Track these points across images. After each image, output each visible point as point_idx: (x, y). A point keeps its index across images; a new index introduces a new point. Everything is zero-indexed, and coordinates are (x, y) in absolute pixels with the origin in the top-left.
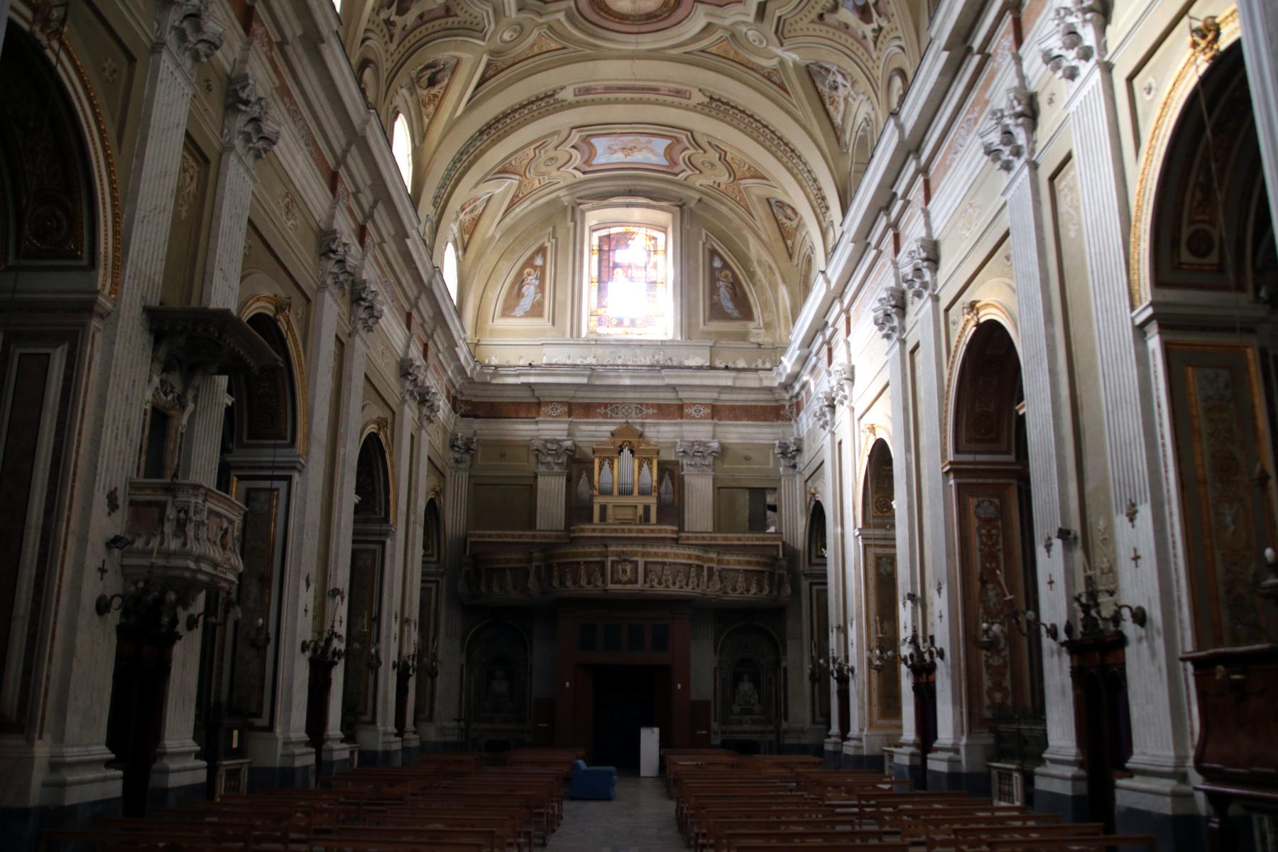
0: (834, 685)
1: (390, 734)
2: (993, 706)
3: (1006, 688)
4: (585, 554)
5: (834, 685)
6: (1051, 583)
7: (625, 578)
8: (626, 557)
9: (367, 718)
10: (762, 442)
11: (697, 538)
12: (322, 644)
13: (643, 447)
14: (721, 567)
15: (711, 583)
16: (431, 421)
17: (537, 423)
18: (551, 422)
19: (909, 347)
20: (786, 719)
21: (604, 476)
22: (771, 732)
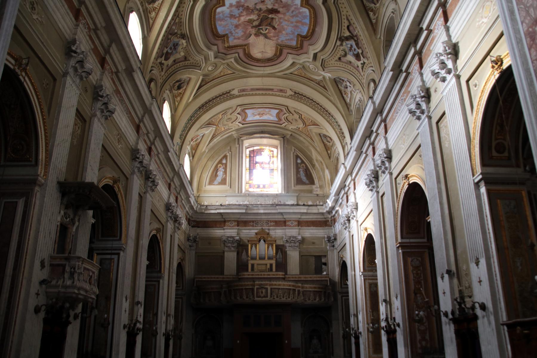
0: (353, 340)
5: (353, 340)
6: (444, 293)
7: (262, 295)
8: (263, 286)
12: (132, 325)
13: (269, 239)
14: (303, 290)
15: (299, 297)
16: (179, 229)
17: (224, 229)
18: (230, 229)
19: (380, 194)
21: (253, 251)
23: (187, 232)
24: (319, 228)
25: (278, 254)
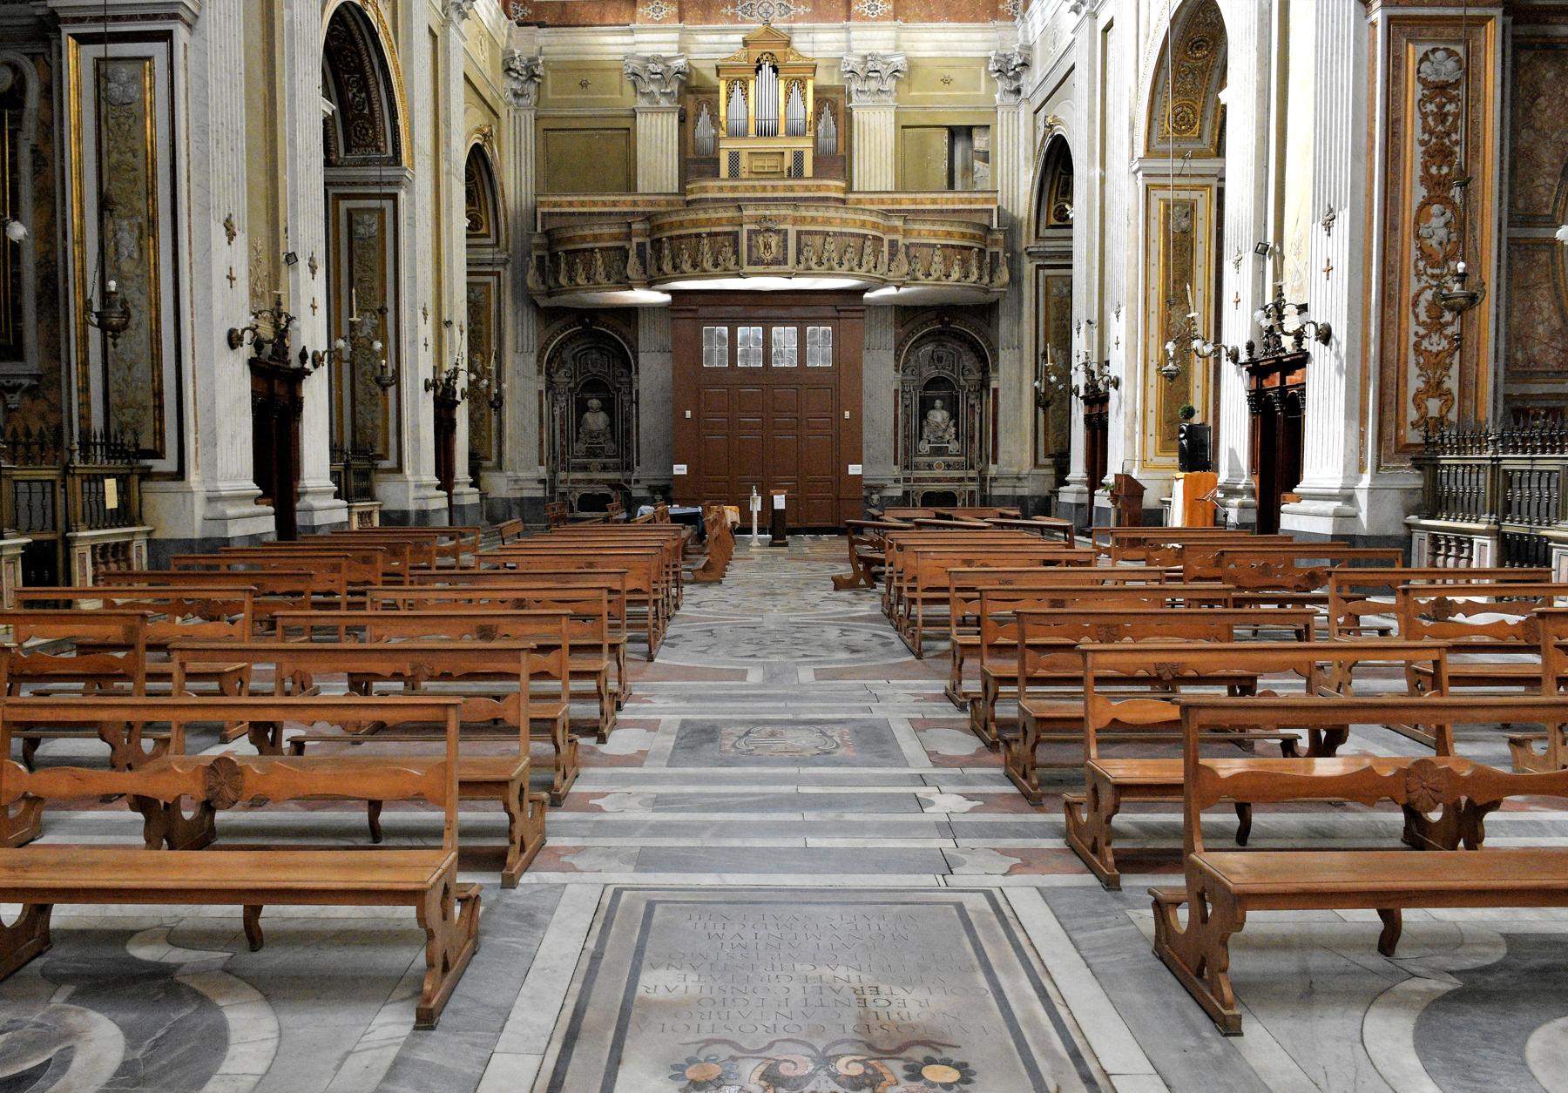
0: (1079, 411)
1: (427, 486)
2: (1424, 422)
3: (1449, 392)
4: (709, 222)
5: (1079, 411)
7: (768, 257)
8: (770, 225)
9: (390, 463)
10: (969, 54)
11: (872, 202)
13: (792, 60)
14: (907, 241)
15: (893, 265)
16: (464, 16)
17: (632, 32)
18: (654, 30)
19: (1101, 24)
20: (995, 461)
21: (733, 108)
22: (972, 479)
23: (502, 41)
24: (969, 25)
25: (822, 121)
